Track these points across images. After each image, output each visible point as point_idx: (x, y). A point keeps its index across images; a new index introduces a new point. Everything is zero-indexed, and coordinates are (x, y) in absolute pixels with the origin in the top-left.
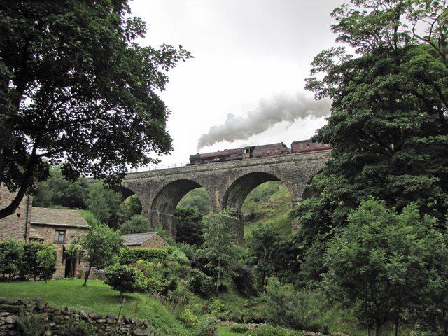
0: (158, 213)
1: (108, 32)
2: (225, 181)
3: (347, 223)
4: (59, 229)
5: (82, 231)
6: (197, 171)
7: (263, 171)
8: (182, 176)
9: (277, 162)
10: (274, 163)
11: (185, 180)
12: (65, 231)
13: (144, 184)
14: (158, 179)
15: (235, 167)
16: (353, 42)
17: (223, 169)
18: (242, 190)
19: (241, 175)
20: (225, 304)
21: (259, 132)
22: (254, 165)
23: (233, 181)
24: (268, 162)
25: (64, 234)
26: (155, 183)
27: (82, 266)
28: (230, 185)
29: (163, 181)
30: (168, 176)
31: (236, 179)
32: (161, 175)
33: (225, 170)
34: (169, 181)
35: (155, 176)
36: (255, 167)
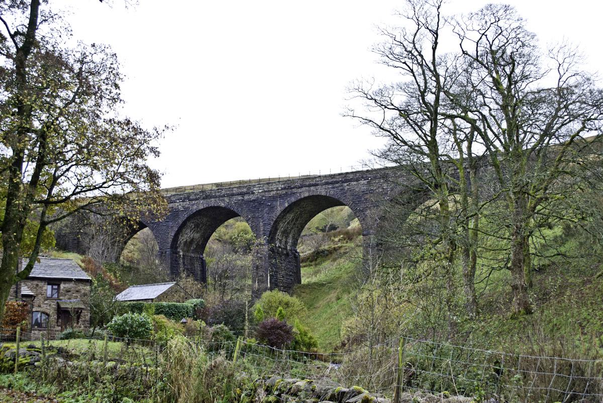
4: (52, 282)
6: (233, 195)
7: (323, 194)
8: (212, 202)
10: (337, 182)
12: (59, 285)
14: (179, 205)
15: (285, 188)
16: (114, 91)
19: (293, 200)
21: (289, 180)
22: (310, 186)
23: (283, 208)
25: (59, 289)
29: (186, 209)
31: (287, 205)
33: (272, 193)
36: (312, 188)
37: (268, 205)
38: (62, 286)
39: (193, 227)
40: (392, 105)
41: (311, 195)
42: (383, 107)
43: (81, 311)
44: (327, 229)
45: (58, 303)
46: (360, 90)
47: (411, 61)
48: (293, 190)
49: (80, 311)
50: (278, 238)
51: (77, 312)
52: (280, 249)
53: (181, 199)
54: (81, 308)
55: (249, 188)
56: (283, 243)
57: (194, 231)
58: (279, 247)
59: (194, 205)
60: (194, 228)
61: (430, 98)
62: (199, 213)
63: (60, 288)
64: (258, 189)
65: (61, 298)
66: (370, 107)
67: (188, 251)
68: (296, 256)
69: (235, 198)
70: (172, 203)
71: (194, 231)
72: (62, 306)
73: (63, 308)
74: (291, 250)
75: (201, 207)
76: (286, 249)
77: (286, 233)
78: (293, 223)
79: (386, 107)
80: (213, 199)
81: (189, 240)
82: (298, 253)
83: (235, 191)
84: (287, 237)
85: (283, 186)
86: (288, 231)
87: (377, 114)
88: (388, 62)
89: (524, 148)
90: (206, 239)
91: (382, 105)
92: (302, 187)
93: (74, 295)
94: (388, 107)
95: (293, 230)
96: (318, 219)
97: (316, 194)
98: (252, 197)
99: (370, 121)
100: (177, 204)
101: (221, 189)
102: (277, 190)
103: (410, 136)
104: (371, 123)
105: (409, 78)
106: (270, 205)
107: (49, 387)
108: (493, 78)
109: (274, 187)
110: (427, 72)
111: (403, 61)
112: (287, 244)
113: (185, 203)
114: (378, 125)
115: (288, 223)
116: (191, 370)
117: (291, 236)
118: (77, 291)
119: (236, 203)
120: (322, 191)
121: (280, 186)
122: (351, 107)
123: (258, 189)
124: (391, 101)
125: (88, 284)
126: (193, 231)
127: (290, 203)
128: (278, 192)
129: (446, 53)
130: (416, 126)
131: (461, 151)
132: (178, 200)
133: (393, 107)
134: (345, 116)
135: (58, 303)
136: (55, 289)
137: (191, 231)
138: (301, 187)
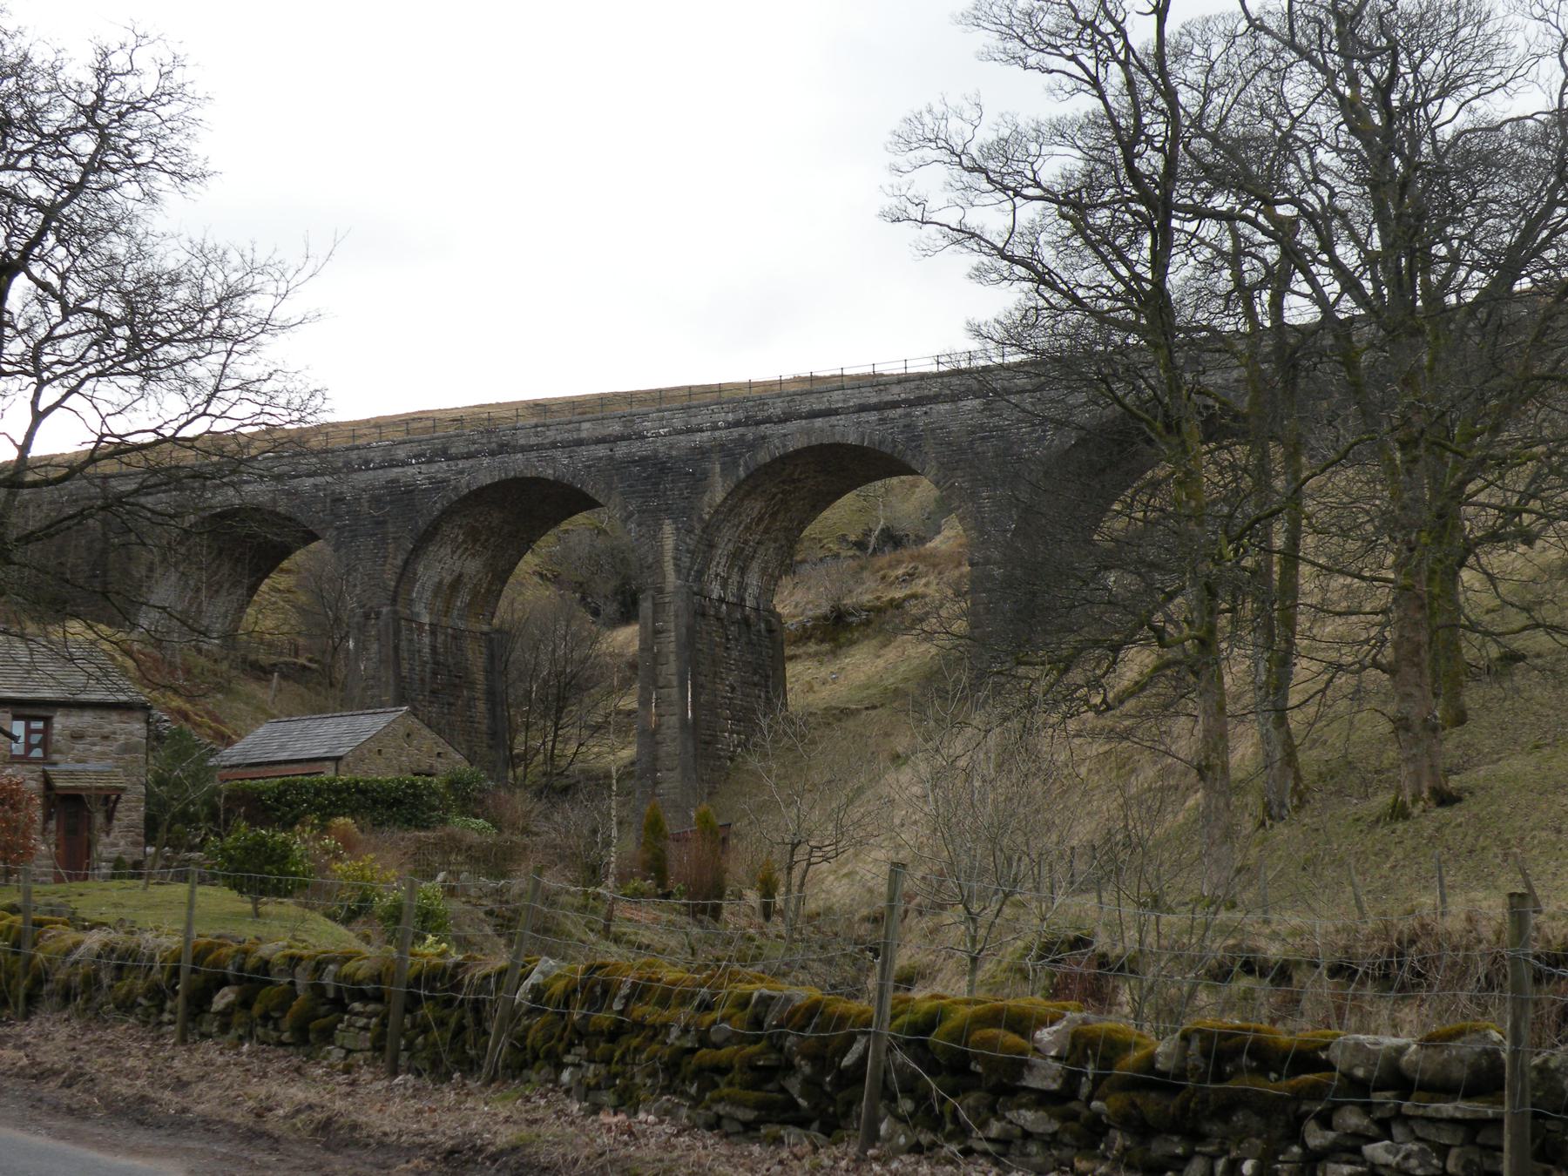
0: (426, 619)
1: (1229, 919)
2: (699, 482)
3: (1423, 926)
4: (28, 712)
5: (114, 716)
6: (580, 443)
7: (852, 439)
8: (517, 465)
9: (910, 403)
10: (895, 405)
11: (538, 481)
12: (47, 720)
13: (357, 499)
14: (416, 474)
15: (737, 424)
17: (690, 431)
18: (774, 515)
19: (763, 457)
20: (425, 782)
22: (813, 415)
24: (874, 400)
25: (46, 732)
26: (403, 496)
27: (115, 842)
28: (719, 498)
29: (438, 484)
30: (461, 464)
31: (742, 473)
32: (430, 461)
34: (465, 484)
35: (404, 464)
36: (818, 422)
37: (689, 473)
38: (60, 722)
39: (461, 538)
40: (1038, 185)
41: (814, 443)
42: (1011, 193)
43: (119, 797)
44: (873, 540)
45: (45, 773)
46: (941, 143)
47: (1091, 53)
48: (762, 427)
49: (114, 797)
50: (717, 575)
51: (107, 798)
52: (724, 607)
53: (424, 456)
54: (118, 788)
55: (627, 419)
56: (733, 588)
57: (464, 553)
58: (721, 600)
59: (461, 472)
60: (464, 542)
61: (1150, 162)
62: (481, 496)
63: (52, 727)
64: (657, 424)
65: (56, 757)
66: (971, 195)
67: (446, 613)
68: (773, 625)
69: (584, 452)
70: (397, 466)
71: (464, 553)
72: (60, 782)
73: (61, 788)
74: (757, 610)
75: (485, 479)
76: (741, 603)
77: (740, 560)
78: (761, 527)
79: (1017, 194)
80: (520, 455)
81: (448, 579)
82: (779, 616)
83: (587, 430)
84: (743, 571)
85: (730, 417)
86: (748, 551)
87: (992, 217)
88: (1022, 55)
89: (1452, 299)
90: (501, 575)
91: (1009, 188)
92: (786, 420)
93: (95, 748)
94: (1026, 192)
95: (761, 550)
96: (844, 513)
97: (831, 441)
98: (638, 450)
99: (973, 235)
100: (410, 471)
101: (544, 425)
102: (715, 428)
103: (1089, 275)
104: (972, 244)
105: (1088, 103)
106: (693, 474)
107: (149, 936)
108: (1341, 97)
109: (702, 419)
110: (1140, 77)
111: (1068, 52)
112: (745, 590)
113: (434, 467)
114: (995, 247)
115: (747, 528)
116: (501, 1141)
117: (755, 566)
118: (105, 738)
119: (590, 467)
120: (847, 431)
121: (721, 418)
122: (916, 191)
123: (657, 424)
124: (1035, 173)
125: (139, 715)
126: (459, 552)
127: (752, 466)
128: (717, 433)
129: (1207, 15)
130: (1101, 245)
131: (1250, 314)
132: (414, 457)
133: (1038, 192)
134: (898, 220)
135: (45, 773)
136: (37, 731)
137: (453, 552)
138: (785, 418)
